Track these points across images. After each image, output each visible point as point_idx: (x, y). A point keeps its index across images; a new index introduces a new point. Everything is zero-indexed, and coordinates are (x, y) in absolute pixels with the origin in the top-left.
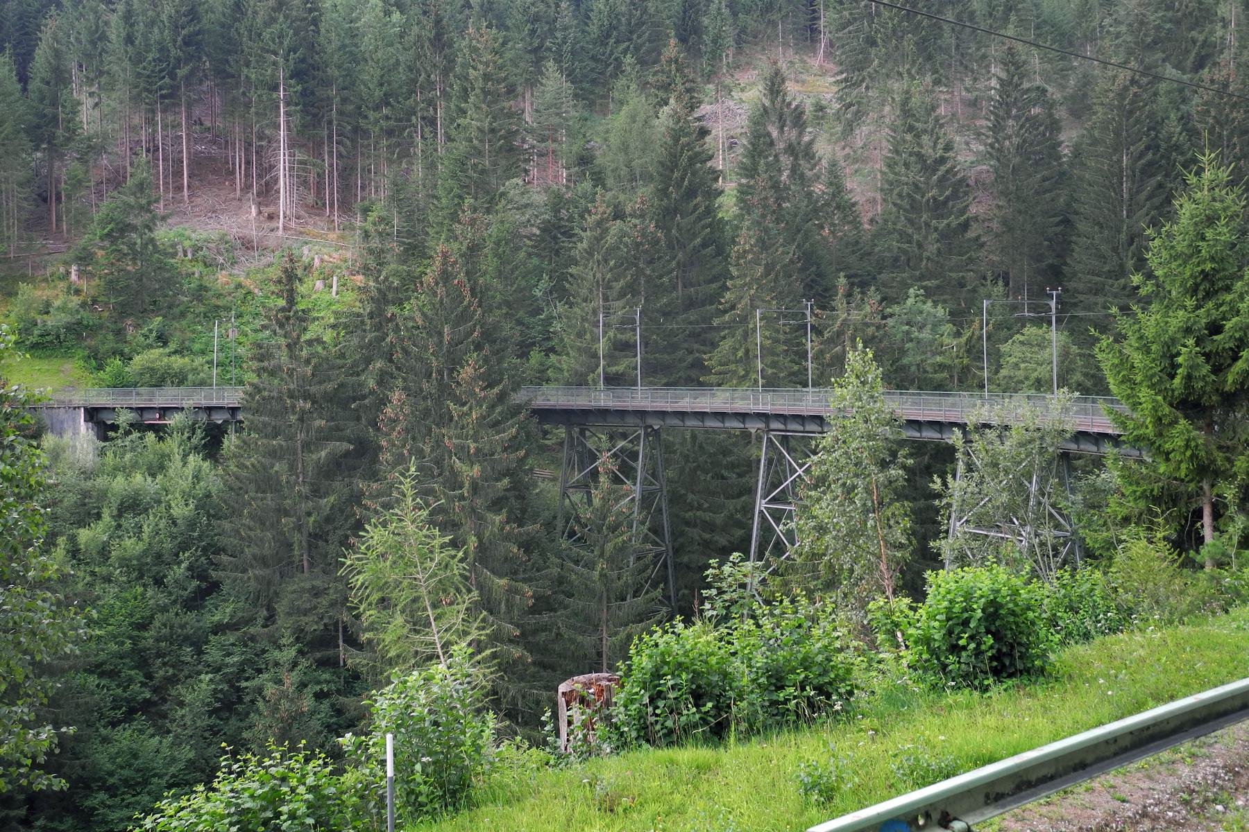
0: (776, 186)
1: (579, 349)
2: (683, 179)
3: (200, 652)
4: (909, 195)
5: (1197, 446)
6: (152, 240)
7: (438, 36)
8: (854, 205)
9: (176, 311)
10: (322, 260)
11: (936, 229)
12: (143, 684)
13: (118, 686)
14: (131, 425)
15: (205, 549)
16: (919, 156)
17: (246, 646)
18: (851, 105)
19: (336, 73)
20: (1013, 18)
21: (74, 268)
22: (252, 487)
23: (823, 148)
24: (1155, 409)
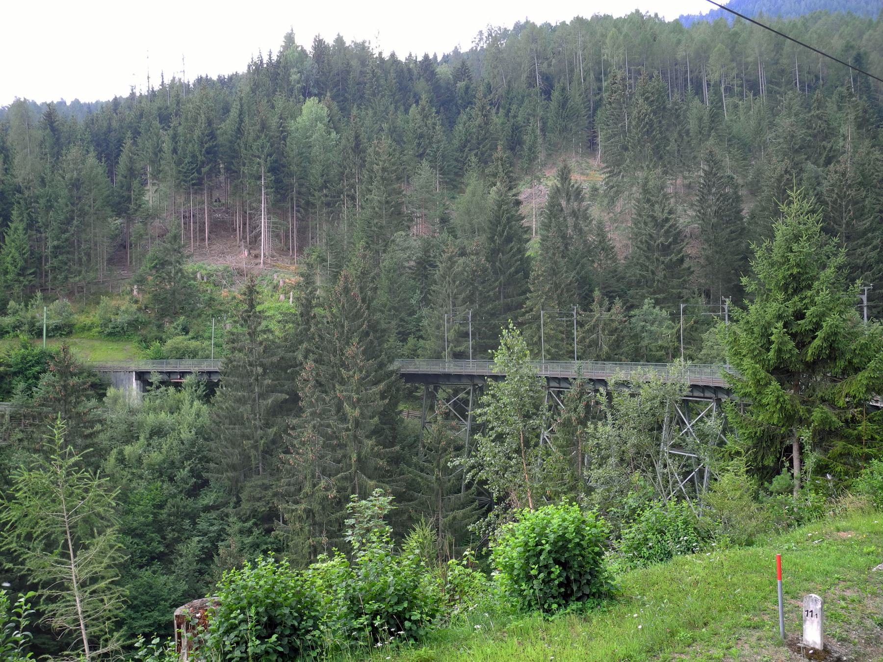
0: (564, 237)
1: (437, 336)
2: (503, 231)
3: (195, 523)
4: (646, 241)
5: (784, 401)
6: (180, 270)
7: (357, 145)
8: (613, 248)
9: (195, 313)
10: (284, 282)
11: (663, 262)
12: (159, 542)
13: (144, 543)
14: (160, 382)
15: (200, 460)
16: (653, 217)
17: (223, 520)
18: (612, 187)
19: (296, 169)
20: (713, 133)
21: (135, 287)
22: (227, 421)
23: (595, 212)
24: (754, 374)
